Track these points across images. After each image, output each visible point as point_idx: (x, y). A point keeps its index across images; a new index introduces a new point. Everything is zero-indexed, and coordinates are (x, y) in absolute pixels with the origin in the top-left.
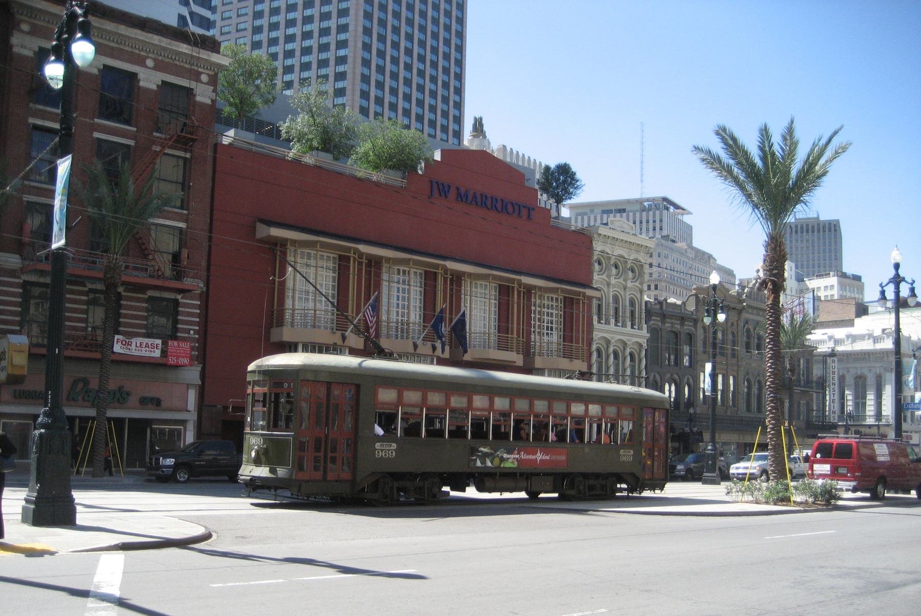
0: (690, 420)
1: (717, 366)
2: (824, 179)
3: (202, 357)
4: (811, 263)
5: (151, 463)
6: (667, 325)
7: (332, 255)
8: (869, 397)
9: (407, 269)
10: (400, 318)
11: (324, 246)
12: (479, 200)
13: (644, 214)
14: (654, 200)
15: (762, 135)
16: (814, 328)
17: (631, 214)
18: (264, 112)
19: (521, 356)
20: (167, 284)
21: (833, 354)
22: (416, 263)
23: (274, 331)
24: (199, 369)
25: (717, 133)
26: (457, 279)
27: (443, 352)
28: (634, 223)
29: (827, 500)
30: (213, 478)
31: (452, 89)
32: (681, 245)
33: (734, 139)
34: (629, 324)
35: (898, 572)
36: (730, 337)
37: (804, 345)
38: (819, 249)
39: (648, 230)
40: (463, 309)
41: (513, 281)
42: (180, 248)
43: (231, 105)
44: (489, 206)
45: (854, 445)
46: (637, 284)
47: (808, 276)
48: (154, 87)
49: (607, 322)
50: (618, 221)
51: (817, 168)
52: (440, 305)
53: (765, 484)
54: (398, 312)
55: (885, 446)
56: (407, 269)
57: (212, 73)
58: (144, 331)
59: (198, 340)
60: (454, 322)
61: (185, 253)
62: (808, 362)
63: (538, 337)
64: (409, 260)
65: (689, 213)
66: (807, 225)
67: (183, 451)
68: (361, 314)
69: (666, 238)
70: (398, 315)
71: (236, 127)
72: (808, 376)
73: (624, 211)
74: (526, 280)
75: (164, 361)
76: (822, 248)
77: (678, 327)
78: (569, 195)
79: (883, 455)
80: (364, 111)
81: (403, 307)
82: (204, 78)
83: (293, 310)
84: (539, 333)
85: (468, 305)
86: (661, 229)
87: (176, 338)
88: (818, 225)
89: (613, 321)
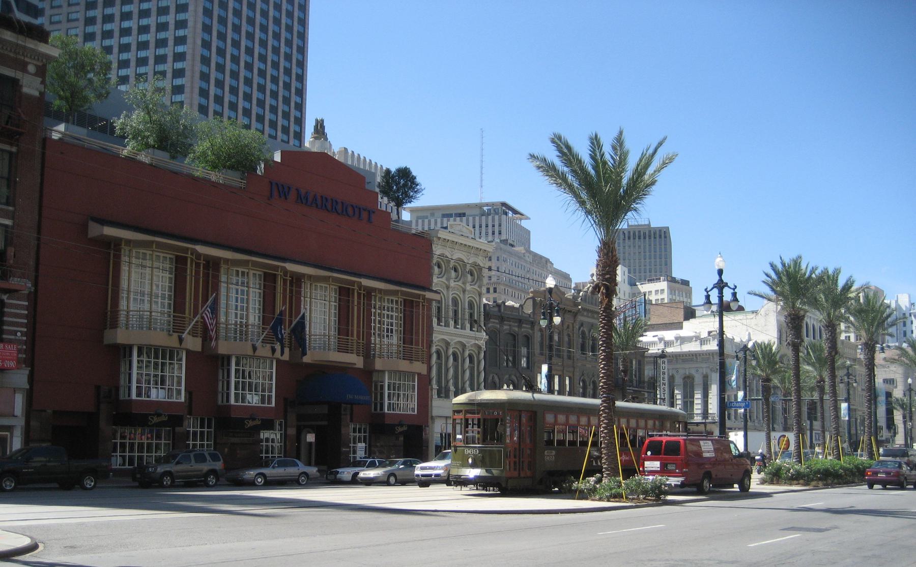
2: (654, 187)
3: (30, 360)
4: (643, 268)
7: (168, 256)
9: (246, 271)
10: (239, 320)
11: (160, 246)
13: (484, 218)
14: (493, 204)
15: (593, 143)
16: (645, 331)
17: (471, 219)
18: (97, 107)
21: (663, 355)
22: (255, 264)
24: (27, 372)
25: (553, 141)
28: (474, 227)
32: (520, 249)
33: (569, 148)
39: (487, 234)
40: (303, 311)
41: (353, 283)
43: (61, 98)
47: (640, 280)
49: (447, 325)
52: (279, 307)
54: (236, 314)
55: (710, 442)
56: (246, 271)
57: (40, 64)
59: (25, 343)
60: (294, 323)
62: (640, 363)
63: (378, 339)
65: (528, 218)
66: (639, 232)
67: (10, 457)
68: (199, 316)
69: (505, 242)
70: (236, 317)
71: (67, 121)
72: (640, 377)
73: (464, 215)
74: (366, 282)
77: (516, 329)
78: (410, 199)
79: (708, 452)
80: (203, 110)
81: (242, 309)
82: (31, 68)
85: (308, 307)
86: (500, 233)
88: (650, 232)
89: (452, 323)
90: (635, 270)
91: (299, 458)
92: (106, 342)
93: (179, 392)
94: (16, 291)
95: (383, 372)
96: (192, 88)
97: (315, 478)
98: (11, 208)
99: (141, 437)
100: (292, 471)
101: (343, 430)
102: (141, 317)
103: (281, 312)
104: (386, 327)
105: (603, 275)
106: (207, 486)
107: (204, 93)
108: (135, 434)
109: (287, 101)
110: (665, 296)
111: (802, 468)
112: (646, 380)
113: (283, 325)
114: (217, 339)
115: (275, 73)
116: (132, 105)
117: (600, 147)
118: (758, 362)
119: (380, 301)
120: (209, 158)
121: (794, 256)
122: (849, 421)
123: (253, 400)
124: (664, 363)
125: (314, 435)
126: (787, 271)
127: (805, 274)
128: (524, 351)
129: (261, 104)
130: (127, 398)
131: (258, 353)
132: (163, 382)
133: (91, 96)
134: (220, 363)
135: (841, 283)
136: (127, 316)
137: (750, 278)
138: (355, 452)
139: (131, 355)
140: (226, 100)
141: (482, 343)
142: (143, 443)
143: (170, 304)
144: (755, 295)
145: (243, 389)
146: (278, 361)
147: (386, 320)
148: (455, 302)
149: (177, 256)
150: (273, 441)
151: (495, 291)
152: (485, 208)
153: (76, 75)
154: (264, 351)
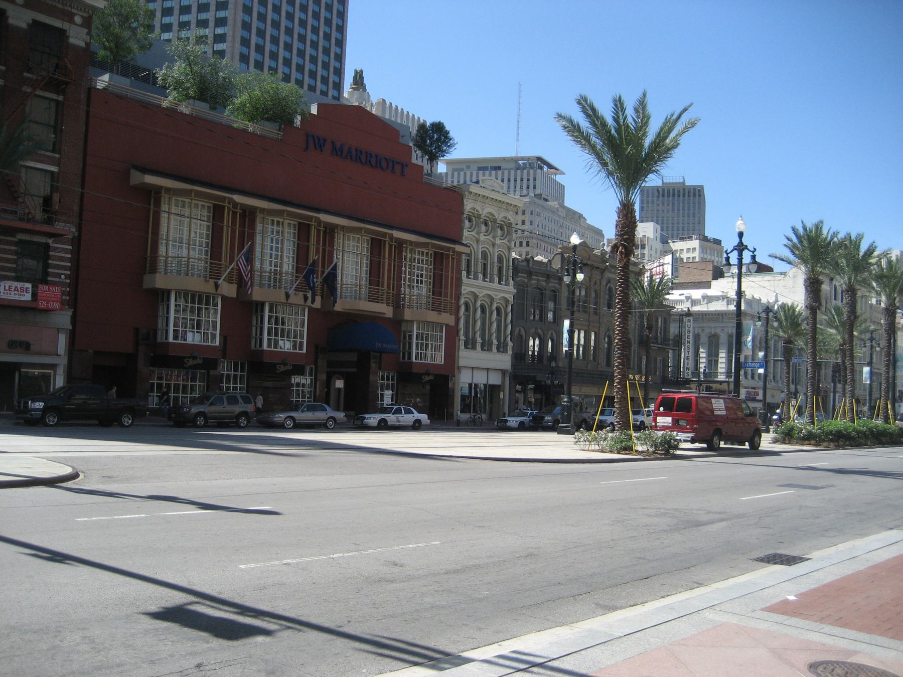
0: (552, 373)
1: (575, 322)
2: (676, 150)
3: (73, 302)
4: (676, 226)
5: (19, 407)
6: (533, 282)
7: (207, 204)
8: (721, 355)
9: (281, 220)
10: (273, 268)
11: (199, 195)
12: (354, 153)
13: (519, 171)
14: (528, 158)
15: (616, 105)
16: (672, 289)
17: (506, 172)
18: (140, 58)
19: (391, 308)
20: (37, 228)
21: (689, 314)
22: (291, 215)
23: (147, 278)
24: (70, 313)
25: (579, 103)
26: (330, 231)
27: (313, 301)
28: (503, 181)
29: (666, 450)
30: (87, 422)
31: (333, 41)
32: (553, 204)
33: (593, 110)
34: (496, 279)
35: (709, 512)
36: (593, 295)
37: (661, 305)
38: (684, 214)
39: (521, 188)
40: (335, 260)
41: (384, 235)
42: (51, 192)
43: (105, 48)
44: (364, 161)
45: (694, 399)
46: (505, 241)
47: (672, 238)
48: (24, 26)
49: (476, 278)
50: (490, 180)
51: (668, 141)
52: (312, 256)
53: (610, 435)
54: (271, 262)
55: (722, 401)
56: (281, 220)
57: (86, 15)
58: (13, 274)
59: (69, 285)
60: (326, 272)
61: (56, 197)
62: (666, 322)
63: (407, 290)
64: (284, 211)
65: (562, 173)
66: (674, 190)
67: (53, 394)
68: (234, 264)
69: (539, 196)
70: (271, 265)
71: (111, 71)
72: (665, 334)
73: (499, 168)
74: (397, 234)
75: (34, 305)
76: (686, 212)
77: (544, 284)
78: (443, 153)
79: (720, 410)
80: (244, 59)
81: (276, 258)
82: (78, 20)
83: (167, 257)
84: (409, 286)
85: (340, 257)
86: (534, 188)
87: (46, 282)
88: (684, 189)
89: (481, 276)
90: (668, 227)
91: (328, 404)
92: (145, 287)
93: (214, 336)
94: (61, 235)
95: (412, 322)
96: (234, 36)
97: (343, 423)
98: (57, 156)
99: (176, 378)
100: (320, 416)
101: (372, 378)
102: (179, 264)
103: (314, 261)
104: (416, 278)
105: (622, 235)
106: (239, 428)
107: (245, 42)
108: (171, 376)
109: (327, 51)
110: (696, 254)
111: (815, 429)
112: (671, 337)
113: (316, 274)
114: (252, 285)
115: (316, 24)
116: (173, 56)
117: (623, 110)
118: (780, 323)
119: (411, 253)
120: (247, 110)
121: (815, 221)
122: (870, 385)
123: (286, 346)
124: (689, 321)
125: (342, 381)
126: (808, 236)
127: (826, 238)
128: (551, 305)
129: (301, 54)
130: (164, 341)
131: (291, 300)
132: (199, 327)
133: (135, 47)
134: (254, 310)
135: (863, 248)
136: (166, 262)
137: (769, 243)
138: (382, 400)
139: (169, 300)
140: (267, 49)
141: (510, 298)
142: (179, 385)
143: (207, 251)
144: (776, 257)
145: (276, 335)
146: (310, 309)
147: (416, 271)
148: (484, 255)
149: (215, 205)
150: (303, 386)
151: (528, 245)
152: (521, 162)
153: (121, 26)
154: (297, 299)
